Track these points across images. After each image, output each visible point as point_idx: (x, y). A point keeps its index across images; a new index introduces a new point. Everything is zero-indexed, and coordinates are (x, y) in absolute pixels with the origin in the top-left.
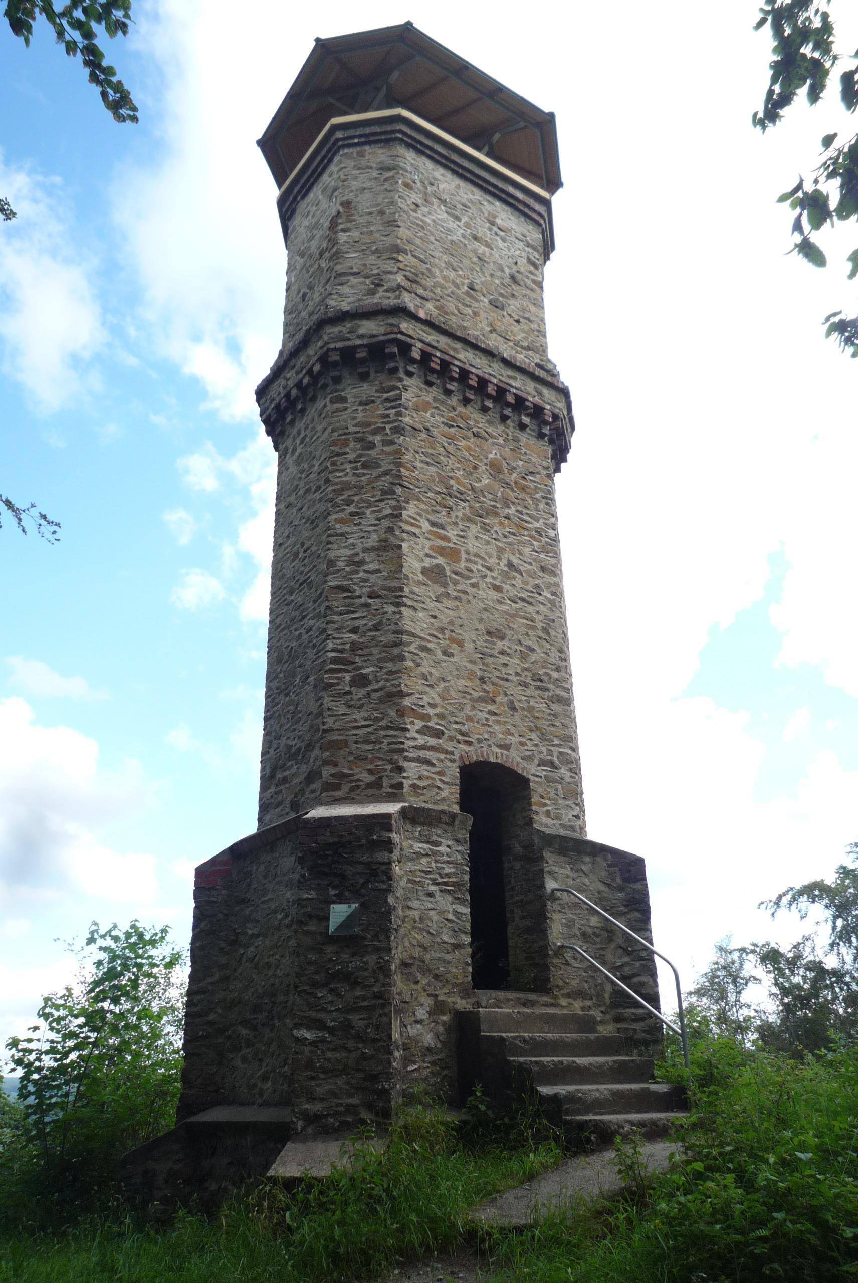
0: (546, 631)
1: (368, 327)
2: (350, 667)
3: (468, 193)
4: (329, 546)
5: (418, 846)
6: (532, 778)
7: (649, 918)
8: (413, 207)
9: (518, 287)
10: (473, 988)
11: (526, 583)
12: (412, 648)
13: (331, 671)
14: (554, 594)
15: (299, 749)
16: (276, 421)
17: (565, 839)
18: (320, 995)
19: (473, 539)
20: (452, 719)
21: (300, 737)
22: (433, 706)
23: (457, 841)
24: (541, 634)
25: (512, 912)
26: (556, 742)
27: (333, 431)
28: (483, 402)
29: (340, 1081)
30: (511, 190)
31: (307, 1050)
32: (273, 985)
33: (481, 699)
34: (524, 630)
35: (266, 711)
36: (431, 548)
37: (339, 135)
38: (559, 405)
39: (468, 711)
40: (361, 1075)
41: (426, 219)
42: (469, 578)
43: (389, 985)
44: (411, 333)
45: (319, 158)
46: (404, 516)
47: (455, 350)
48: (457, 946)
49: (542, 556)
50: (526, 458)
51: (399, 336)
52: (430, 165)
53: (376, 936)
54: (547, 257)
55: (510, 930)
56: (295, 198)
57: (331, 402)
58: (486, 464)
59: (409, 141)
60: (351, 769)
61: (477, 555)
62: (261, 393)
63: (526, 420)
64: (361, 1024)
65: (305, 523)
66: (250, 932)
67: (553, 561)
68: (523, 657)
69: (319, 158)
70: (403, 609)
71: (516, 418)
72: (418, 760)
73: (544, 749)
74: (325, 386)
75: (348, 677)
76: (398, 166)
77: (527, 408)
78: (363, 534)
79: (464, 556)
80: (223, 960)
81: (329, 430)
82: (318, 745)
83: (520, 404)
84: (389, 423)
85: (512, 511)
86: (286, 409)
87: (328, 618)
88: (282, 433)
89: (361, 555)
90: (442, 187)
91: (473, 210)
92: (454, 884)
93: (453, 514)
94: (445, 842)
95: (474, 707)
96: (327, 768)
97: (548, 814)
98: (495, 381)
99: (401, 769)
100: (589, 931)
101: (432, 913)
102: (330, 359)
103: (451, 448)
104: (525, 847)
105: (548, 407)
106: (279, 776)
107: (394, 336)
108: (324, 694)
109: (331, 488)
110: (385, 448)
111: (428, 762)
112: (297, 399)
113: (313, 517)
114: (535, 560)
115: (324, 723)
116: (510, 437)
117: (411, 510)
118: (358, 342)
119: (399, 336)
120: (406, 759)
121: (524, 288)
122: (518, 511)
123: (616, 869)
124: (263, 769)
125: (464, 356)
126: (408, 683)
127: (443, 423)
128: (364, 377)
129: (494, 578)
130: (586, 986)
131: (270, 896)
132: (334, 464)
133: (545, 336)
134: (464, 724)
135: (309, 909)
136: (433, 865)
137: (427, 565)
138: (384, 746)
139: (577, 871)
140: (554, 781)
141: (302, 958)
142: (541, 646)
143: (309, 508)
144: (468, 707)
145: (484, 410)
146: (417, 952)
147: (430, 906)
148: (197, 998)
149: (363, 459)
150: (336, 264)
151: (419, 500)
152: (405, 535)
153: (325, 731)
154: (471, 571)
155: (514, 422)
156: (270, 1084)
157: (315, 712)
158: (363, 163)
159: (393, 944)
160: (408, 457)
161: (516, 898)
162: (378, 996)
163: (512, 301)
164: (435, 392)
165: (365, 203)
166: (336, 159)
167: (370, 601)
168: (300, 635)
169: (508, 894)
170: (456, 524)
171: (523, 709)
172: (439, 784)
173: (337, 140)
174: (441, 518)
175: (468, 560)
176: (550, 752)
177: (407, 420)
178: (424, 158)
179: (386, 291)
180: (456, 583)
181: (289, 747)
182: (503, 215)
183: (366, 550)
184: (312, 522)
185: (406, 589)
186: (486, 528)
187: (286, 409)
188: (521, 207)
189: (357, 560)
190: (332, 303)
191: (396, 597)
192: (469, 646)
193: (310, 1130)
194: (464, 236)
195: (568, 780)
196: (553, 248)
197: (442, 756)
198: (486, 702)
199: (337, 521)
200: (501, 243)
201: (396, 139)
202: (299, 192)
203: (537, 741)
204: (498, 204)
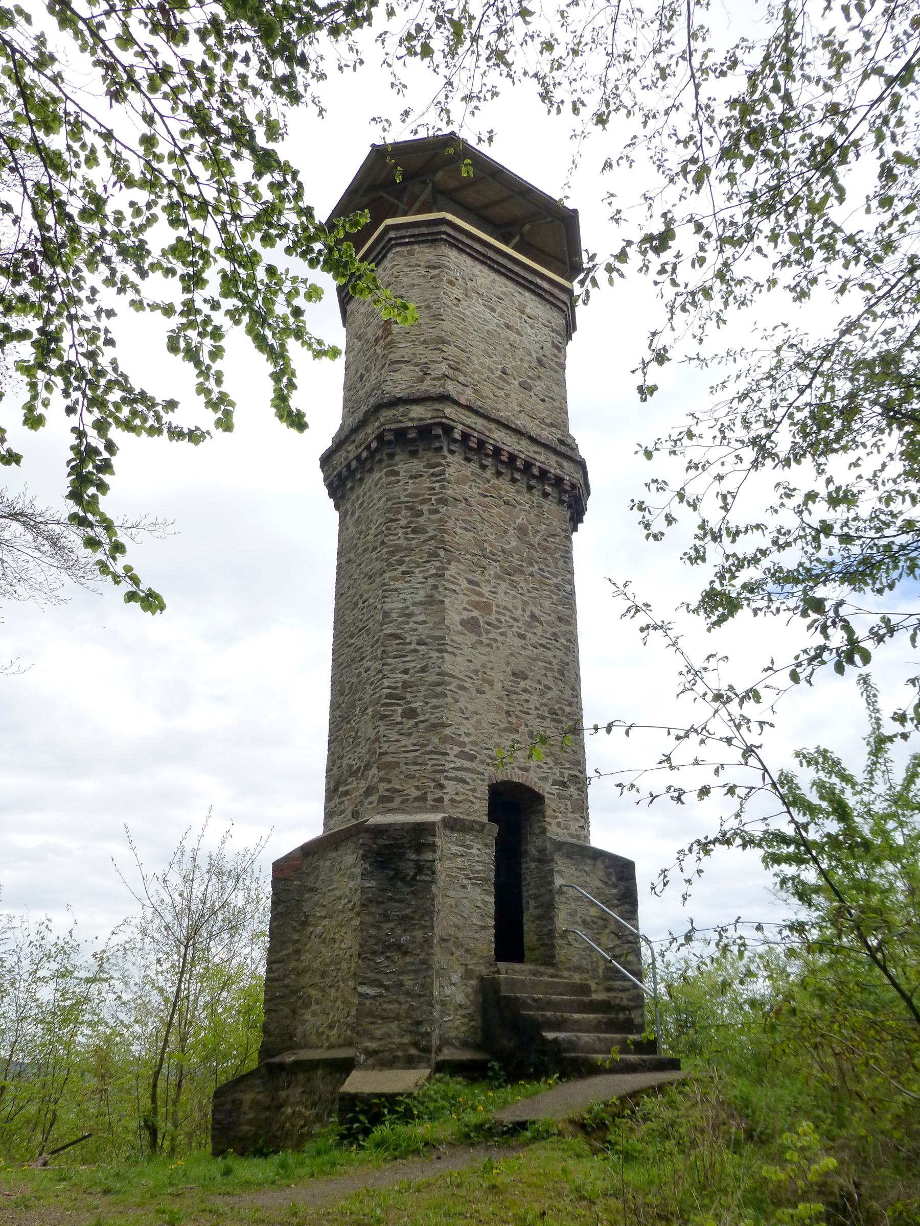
0: (561, 672)
1: (418, 412)
2: (401, 702)
3: (503, 286)
5: (455, 849)
6: (546, 795)
7: (636, 910)
8: (455, 302)
9: (543, 370)
11: (545, 631)
12: (452, 687)
14: (569, 640)
15: (359, 768)
16: (338, 487)
17: (572, 845)
22: (468, 735)
23: (486, 845)
24: (557, 675)
25: (528, 903)
26: (567, 765)
27: (387, 500)
29: (394, 1026)
30: (538, 281)
31: (368, 1002)
33: (506, 730)
34: (543, 672)
35: (330, 735)
36: (469, 603)
37: (392, 234)
38: (577, 476)
39: (495, 739)
40: (409, 1021)
42: (499, 628)
43: (432, 954)
44: (454, 417)
46: (447, 576)
47: (490, 430)
48: (484, 928)
49: (560, 608)
51: (444, 420)
52: (469, 262)
53: (422, 917)
54: (569, 337)
55: (526, 917)
57: (386, 475)
61: (505, 608)
62: (326, 460)
63: (548, 489)
64: (410, 983)
67: (569, 612)
68: (542, 694)
71: (540, 487)
72: (455, 779)
73: (557, 772)
74: (380, 461)
75: (399, 709)
77: (550, 479)
79: (494, 609)
80: (296, 937)
81: (384, 499)
82: (375, 766)
83: (543, 475)
85: (535, 569)
86: (347, 478)
88: (343, 497)
90: (479, 282)
91: (507, 302)
92: (483, 879)
94: (476, 846)
95: (500, 736)
97: (559, 824)
99: (442, 787)
100: (589, 919)
101: (465, 901)
103: (485, 515)
104: (539, 851)
105: (567, 478)
106: (341, 789)
108: (379, 723)
110: (432, 517)
111: (463, 781)
112: (356, 469)
115: (380, 748)
117: (452, 570)
118: (410, 424)
120: (446, 778)
124: (328, 783)
125: (499, 436)
126: (451, 716)
128: (414, 454)
129: (519, 628)
130: (584, 962)
131: (335, 886)
132: (388, 529)
133: (566, 413)
140: (564, 798)
142: (557, 685)
144: (496, 736)
145: (514, 481)
146: (453, 931)
148: (275, 966)
151: (459, 561)
152: (447, 592)
154: (501, 622)
157: (373, 737)
158: (413, 261)
159: (435, 924)
160: (451, 523)
162: (423, 962)
163: (538, 383)
164: (474, 466)
166: (390, 256)
168: (360, 673)
169: (524, 889)
170: (489, 581)
172: (472, 799)
173: (391, 239)
174: (476, 577)
175: (498, 612)
176: (562, 775)
177: (450, 492)
178: (465, 256)
179: (433, 379)
180: (488, 632)
181: (350, 766)
182: (532, 304)
183: (414, 604)
184: (370, 578)
185: (448, 638)
186: (514, 585)
187: (347, 478)
188: (547, 296)
190: (387, 389)
192: (498, 685)
193: (370, 1061)
194: (498, 325)
195: (576, 797)
196: (575, 329)
197: (475, 776)
199: (391, 578)
200: (529, 330)
201: (442, 239)
203: (551, 764)
204: (527, 294)
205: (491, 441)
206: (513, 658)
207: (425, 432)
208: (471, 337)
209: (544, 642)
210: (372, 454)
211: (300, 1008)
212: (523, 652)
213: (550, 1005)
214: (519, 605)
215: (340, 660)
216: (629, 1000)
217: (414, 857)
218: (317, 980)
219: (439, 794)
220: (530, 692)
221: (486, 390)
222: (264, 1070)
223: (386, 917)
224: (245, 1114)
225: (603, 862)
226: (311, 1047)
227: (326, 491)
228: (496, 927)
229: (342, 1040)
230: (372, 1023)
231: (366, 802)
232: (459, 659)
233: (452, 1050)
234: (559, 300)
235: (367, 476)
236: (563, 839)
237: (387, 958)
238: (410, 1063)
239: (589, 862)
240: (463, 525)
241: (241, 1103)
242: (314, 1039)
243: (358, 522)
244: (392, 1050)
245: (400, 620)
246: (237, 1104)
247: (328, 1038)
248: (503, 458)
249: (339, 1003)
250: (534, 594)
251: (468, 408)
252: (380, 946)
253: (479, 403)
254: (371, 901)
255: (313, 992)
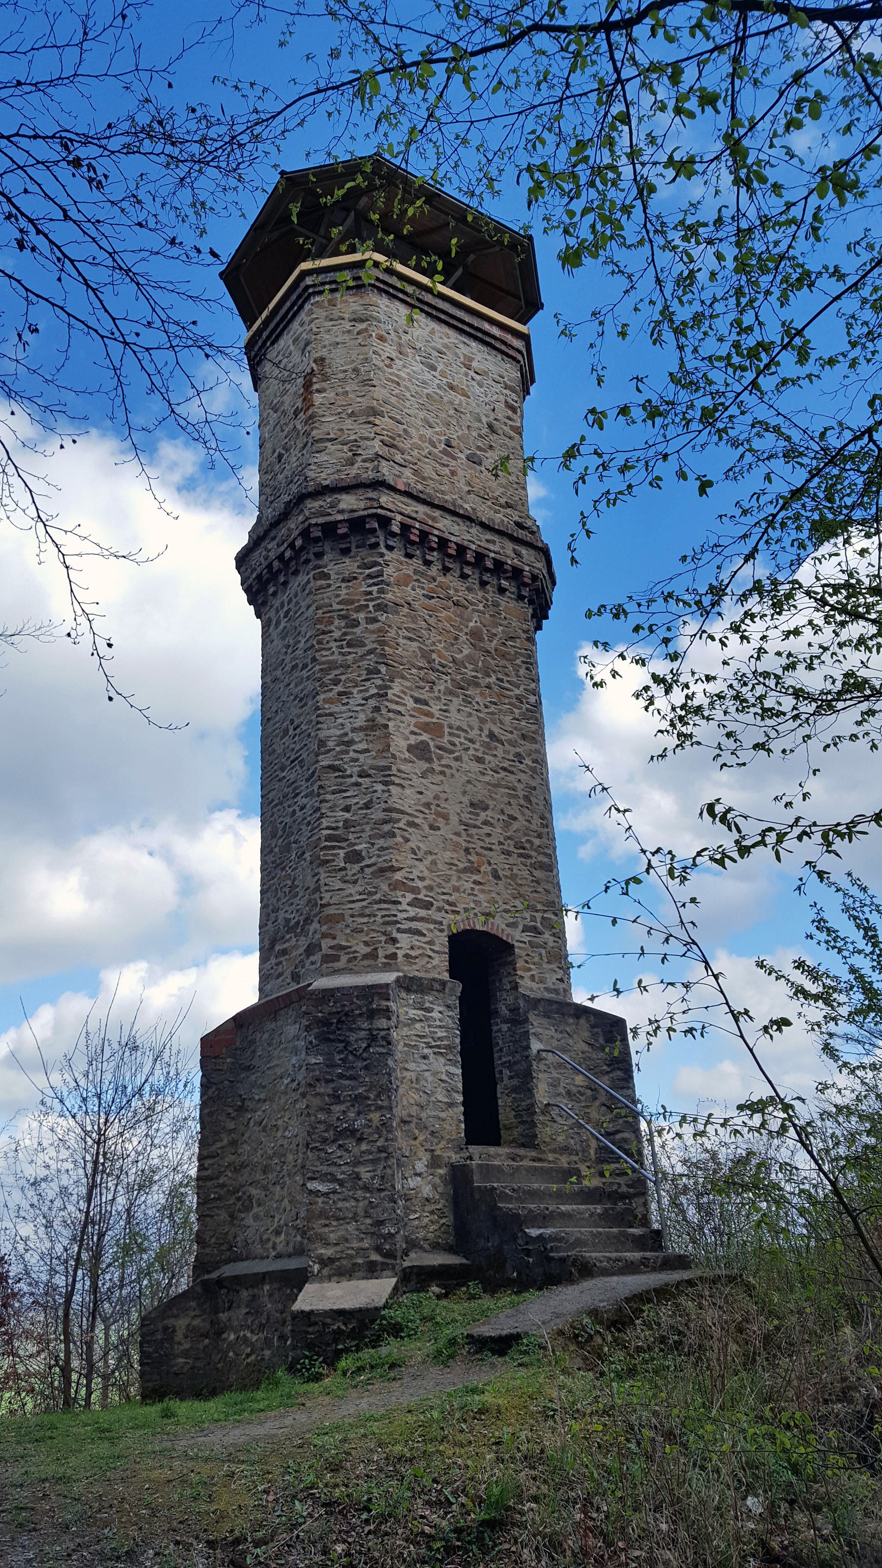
0: (527, 798)
1: (349, 502)
2: (344, 844)
4: (320, 726)
5: (413, 1013)
6: (516, 944)
8: (388, 362)
10: (467, 1144)
12: (401, 825)
13: (325, 848)
14: (535, 761)
15: (298, 923)
16: (258, 592)
17: (550, 1002)
18: (330, 1151)
19: (456, 712)
20: (440, 891)
21: (297, 911)
22: (422, 879)
23: (448, 1007)
25: (501, 1072)
28: (462, 569)
30: (486, 326)
31: (320, 1200)
32: (282, 1146)
33: (465, 870)
34: (506, 799)
35: (262, 885)
37: (309, 281)
38: (539, 565)
39: (454, 882)
41: (400, 373)
42: (452, 752)
44: (390, 506)
45: (288, 304)
46: (390, 696)
47: (434, 519)
49: (523, 723)
50: (506, 622)
51: (379, 511)
53: (378, 1096)
55: (499, 1089)
56: (264, 343)
58: (466, 634)
59: (382, 286)
60: (348, 941)
61: (459, 728)
62: (242, 560)
65: (294, 700)
66: (257, 1097)
67: (534, 727)
68: (506, 825)
69: (288, 304)
70: (391, 787)
72: (410, 931)
74: (307, 561)
75: (342, 853)
76: (371, 316)
77: (506, 571)
78: (351, 714)
79: (447, 730)
80: (231, 1125)
81: (313, 607)
82: (316, 919)
84: (372, 600)
85: (493, 679)
86: (268, 581)
87: (321, 797)
88: (264, 603)
89: (350, 735)
90: (416, 334)
91: (450, 356)
92: (446, 1047)
93: (436, 689)
95: (459, 878)
96: (327, 940)
97: (532, 978)
98: (473, 547)
99: (394, 941)
100: (574, 1089)
101: (427, 1074)
102: (312, 535)
103: (432, 621)
105: (527, 568)
106: (278, 948)
107: (374, 511)
109: (318, 667)
112: (279, 571)
113: (302, 695)
114: (516, 728)
115: (321, 898)
116: (490, 603)
117: (396, 688)
118: (340, 517)
119: (379, 511)
120: (399, 930)
121: (503, 437)
122: (498, 679)
123: (599, 1030)
125: (445, 525)
127: (424, 595)
129: (476, 750)
130: (572, 1142)
131: (275, 1062)
132: (320, 642)
134: (451, 895)
135: (317, 1073)
136: (427, 1030)
137: (413, 743)
138: (379, 919)
139: (561, 1032)
140: (538, 946)
141: (313, 1118)
143: (296, 686)
144: (454, 878)
145: (464, 576)
146: (414, 1110)
147: (425, 1067)
148: (207, 1162)
149: (348, 638)
150: (312, 429)
151: (403, 677)
152: (391, 715)
153: (322, 906)
154: (454, 745)
155: (493, 585)
156: (283, 1236)
157: (312, 887)
158: (336, 313)
159: (394, 1103)
160: (392, 633)
161: (504, 1059)
162: (381, 1150)
163: (489, 454)
165: (338, 360)
166: (307, 307)
167: (360, 780)
168: (294, 812)
169: (496, 1055)
170: (439, 698)
171: (506, 877)
173: (307, 287)
174: (424, 695)
175: (450, 734)
176: (533, 919)
177: (389, 596)
178: (397, 303)
179: (364, 461)
180: (440, 758)
181: (288, 921)
182: (479, 356)
183: (354, 730)
184: (301, 700)
185: (394, 768)
186: (467, 700)
189: (346, 739)
190: (311, 474)
191: (385, 776)
192: (454, 819)
193: (325, 1272)
195: (551, 944)
197: (432, 926)
198: (472, 873)
200: (478, 390)
202: (268, 338)
204: (474, 344)
205: (436, 532)
206: (470, 786)
207: (357, 524)
208: (408, 404)
209: (506, 764)
210: (298, 552)
211: (240, 1211)
212: (482, 778)
213: (534, 1194)
214: (476, 724)
215: (270, 796)
216: (628, 1186)
217: (365, 1025)
218: (259, 1176)
219: (391, 950)
220: (491, 825)
221: (428, 470)
222: (199, 1289)
223: (336, 1098)
224: (179, 1343)
225: (588, 1021)
226: (256, 1258)
227: (244, 596)
228: (464, 1104)
229: (290, 1249)
230: (326, 1225)
231: (308, 963)
232: (408, 791)
233: (421, 1254)
234: (513, 348)
235: (292, 579)
236: (539, 996)
237: (340, 1146)
238: (372, 1270)
239: (571, 1020)
240: (407, 634)
241: (174, 1331)
242: (258, 1249)
243: (284, 635)
244: (351, 1257)
245: (338, 749)
246: (169, 1333)
247: (275, 1244)
248: (450, 551)
249: (286, 1202)
250: (492, 709)
251: (408, 494)
252: (331, 1133)
253: (420, 487)
254: (318, 1080)
255: (254, 1191)
